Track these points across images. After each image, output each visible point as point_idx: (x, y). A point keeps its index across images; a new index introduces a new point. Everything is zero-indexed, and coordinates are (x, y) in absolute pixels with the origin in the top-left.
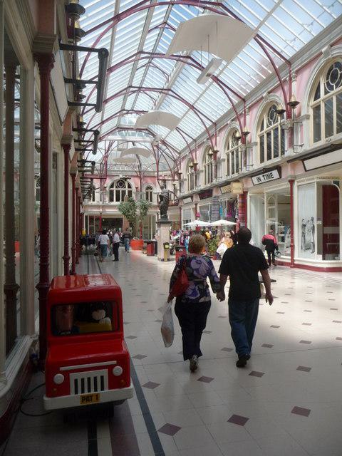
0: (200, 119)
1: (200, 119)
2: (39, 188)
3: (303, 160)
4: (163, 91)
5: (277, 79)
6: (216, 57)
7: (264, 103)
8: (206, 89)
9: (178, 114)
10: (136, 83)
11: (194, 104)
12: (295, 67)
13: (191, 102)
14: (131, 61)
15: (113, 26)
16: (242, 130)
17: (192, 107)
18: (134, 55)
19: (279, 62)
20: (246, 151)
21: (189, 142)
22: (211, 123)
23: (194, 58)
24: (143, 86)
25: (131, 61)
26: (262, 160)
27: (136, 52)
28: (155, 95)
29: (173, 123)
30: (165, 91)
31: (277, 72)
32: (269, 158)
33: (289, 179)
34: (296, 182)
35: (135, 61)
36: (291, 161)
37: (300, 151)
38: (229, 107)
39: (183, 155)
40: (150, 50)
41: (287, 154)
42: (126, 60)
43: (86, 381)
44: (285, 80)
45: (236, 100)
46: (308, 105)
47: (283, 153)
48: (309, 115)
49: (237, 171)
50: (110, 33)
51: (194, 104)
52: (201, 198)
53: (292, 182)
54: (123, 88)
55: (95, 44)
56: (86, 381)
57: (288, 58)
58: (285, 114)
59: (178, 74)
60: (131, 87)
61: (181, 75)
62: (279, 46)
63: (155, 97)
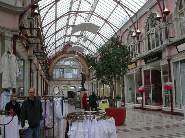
3: (176, 46)
4: (90, 13)
7: (148, 15)
8: (96, 35)
10: (74, 9)
11: (108, 19)
13: (106, 18)
14: (64, 38)
15: (56, 34)
16: (136, 31)
17: (106, 21)
18: (65, 26)
20: (139, 44)
21: (116, 31)
22: (118, 30)
23: (96, 12)
24: (79, 11)
25: (64, 38)
26: (149, 49)
27: (66, 25)
28: (85, 15)
29: (95, 29)
30: (91, 13)
32: (154, 47)
33: (167, 58)
34: (172, 60)
36: (168, 46)
37: (173, 40)
38: (128, 19)
40: (76, 10)
41: (164, 43)
44: (135, 22)
46: (145, 34)
47: (162, 43)
48: (146, 38)
49: (135, 56)
51: (108, 19)
52: (146, 63)
53: (169, 60)
54: (64, 26)
57: (135, 12)
58: (161, 20)
60: (68, 25)
62: (115, 23)
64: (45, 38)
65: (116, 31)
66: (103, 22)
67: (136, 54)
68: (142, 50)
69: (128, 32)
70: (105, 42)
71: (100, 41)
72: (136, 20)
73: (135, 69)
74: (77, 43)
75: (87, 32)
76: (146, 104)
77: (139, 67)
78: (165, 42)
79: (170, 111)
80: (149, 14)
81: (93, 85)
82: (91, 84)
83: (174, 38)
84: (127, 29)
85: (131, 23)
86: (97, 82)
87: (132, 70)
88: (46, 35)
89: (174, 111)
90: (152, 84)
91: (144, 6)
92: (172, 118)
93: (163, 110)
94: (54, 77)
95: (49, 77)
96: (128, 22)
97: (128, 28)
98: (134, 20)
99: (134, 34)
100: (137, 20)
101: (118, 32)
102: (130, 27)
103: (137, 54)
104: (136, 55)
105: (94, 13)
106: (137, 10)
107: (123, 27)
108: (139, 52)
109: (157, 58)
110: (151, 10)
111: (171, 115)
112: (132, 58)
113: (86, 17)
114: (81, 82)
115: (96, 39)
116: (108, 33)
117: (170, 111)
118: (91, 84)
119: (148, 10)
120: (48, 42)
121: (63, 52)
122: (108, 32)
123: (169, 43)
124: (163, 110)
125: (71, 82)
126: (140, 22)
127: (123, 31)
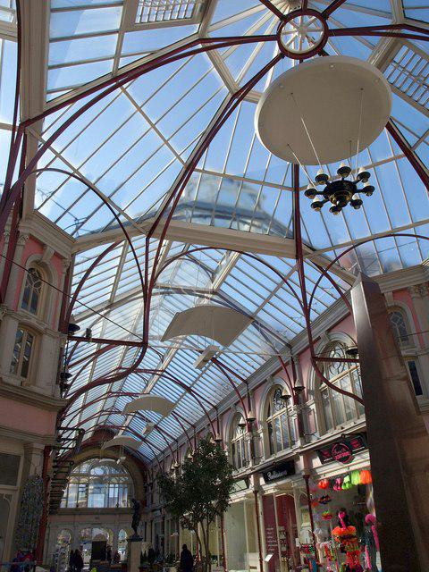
0: (227, 375)
1: (227, 375)
2: (380, 524)
5: (237, 395)
6: (216, 344)
7: (268, 386)
8: (200, 376)
9: (172, 399)
12: (251, 387)
15: (96, 357)
19: (170, 441)
29: (166, 407)
31: (237, 390)
35: (106, 398)
39: (180, 442)
42: (131, 296)
43: (218, 214)
44: (244, 397)
45: (170, 441)
50: (92, 363)
55: (77, 344)
56: (218, 214)
57: (245, 378)
58: (291, 400)
59: (230, 270)
61: (234, 272)
62: (204, 394)
63: (213, 265)
64: (70, 363)
65: (208, 409)
69: (231, 414)
70: (340, 292)
71: (172, 427)
73: (275, 484)
75: (195, 337)
80: (270, 385)
82: (149, 524)
84: (266, 380)
85: (236, 398)
86: (163, 518)
87: (238, 495)
88: (72, 353)
94: (63, 505)
95: (69, 328)
96: (230, 396)
98: (213, 417)
99: (242, 421)
101: (241, 386)
106: (248, 375)
107: (222, 403)
109: (285, 473)
112: (240, 467)
113: (164, 351)
114: (130, 518)
115: (211, 374)
116: (209, 395)
118: (149, 524)
119: (268, 377)
120: (89, 271)
121: (94, 444)
122: (190, 409)
125: (102, 517)
127: (221, 410)
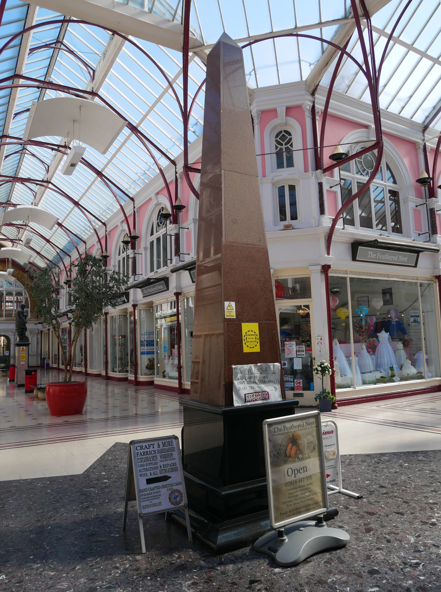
17: (76, 204)
26: (152, 270)
66: (71, 205)
67: (169, 257)
68: (183, 248)
72: (85, 251)
74: (43, 181)
76: (91, 368)
77: (175, 291)
78: (131, 281)
79: (177, 386)
81: (43, 334)
83: (189, 254)
89: (89, 372)
90: (116, 338)
91: (113, 215)
92: (135, 390)
93: (155, 383)
96: (152, 181)
97: (153, 196)
100: (134, 211)
102: (158, 194)
103: (171, 260)
104: (169, 261)
105: (50, 186)
108: (178, 252)
110: (159, 196)
111: (106, 380)
117: (177, 386)
123: (181, 264)
124: (156, 383)
126: (139, 216)
